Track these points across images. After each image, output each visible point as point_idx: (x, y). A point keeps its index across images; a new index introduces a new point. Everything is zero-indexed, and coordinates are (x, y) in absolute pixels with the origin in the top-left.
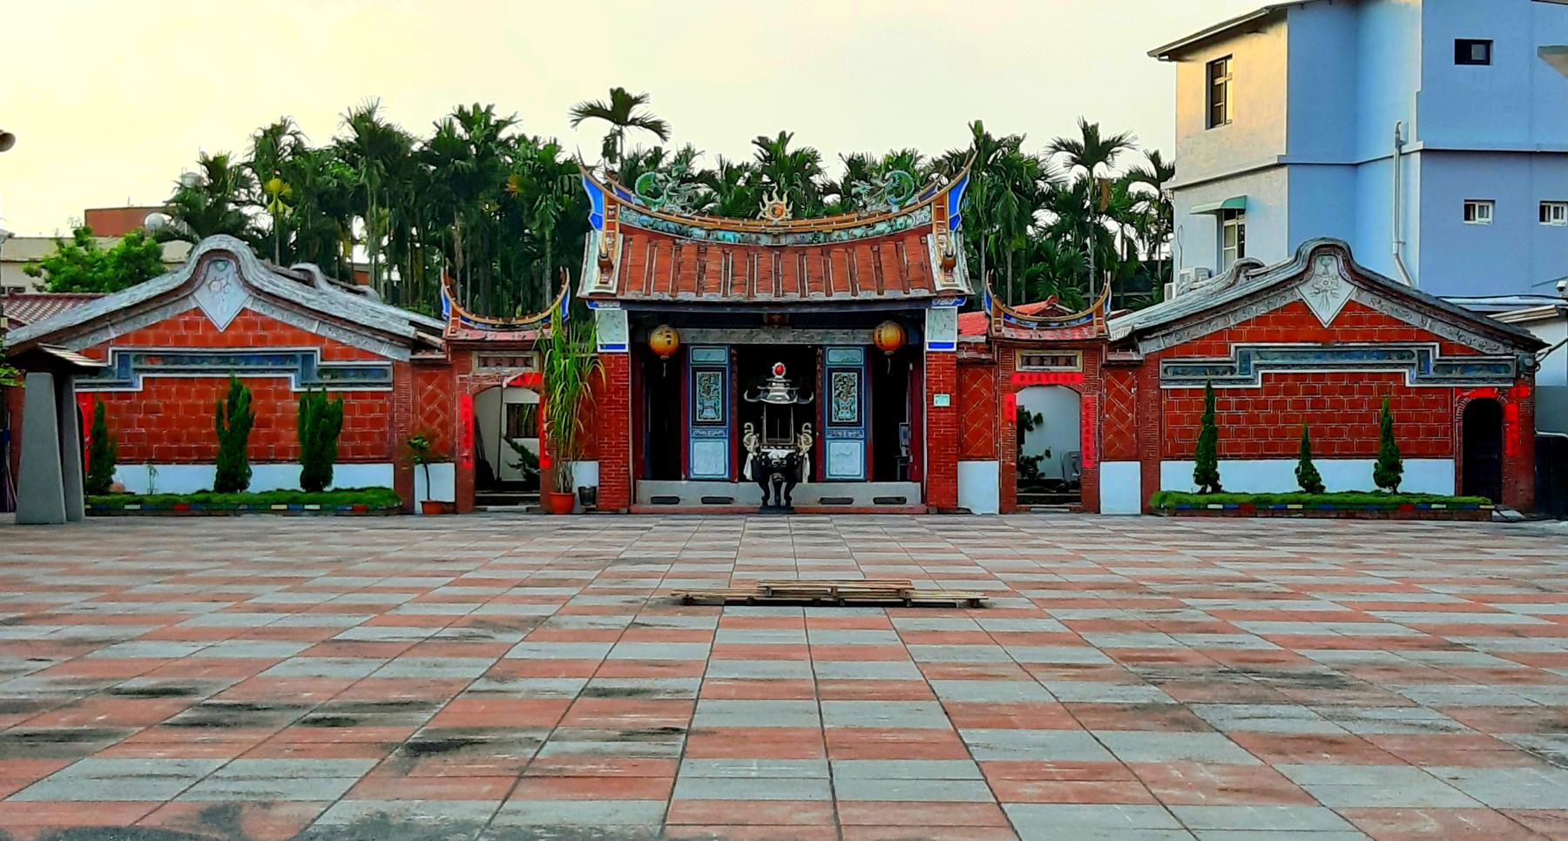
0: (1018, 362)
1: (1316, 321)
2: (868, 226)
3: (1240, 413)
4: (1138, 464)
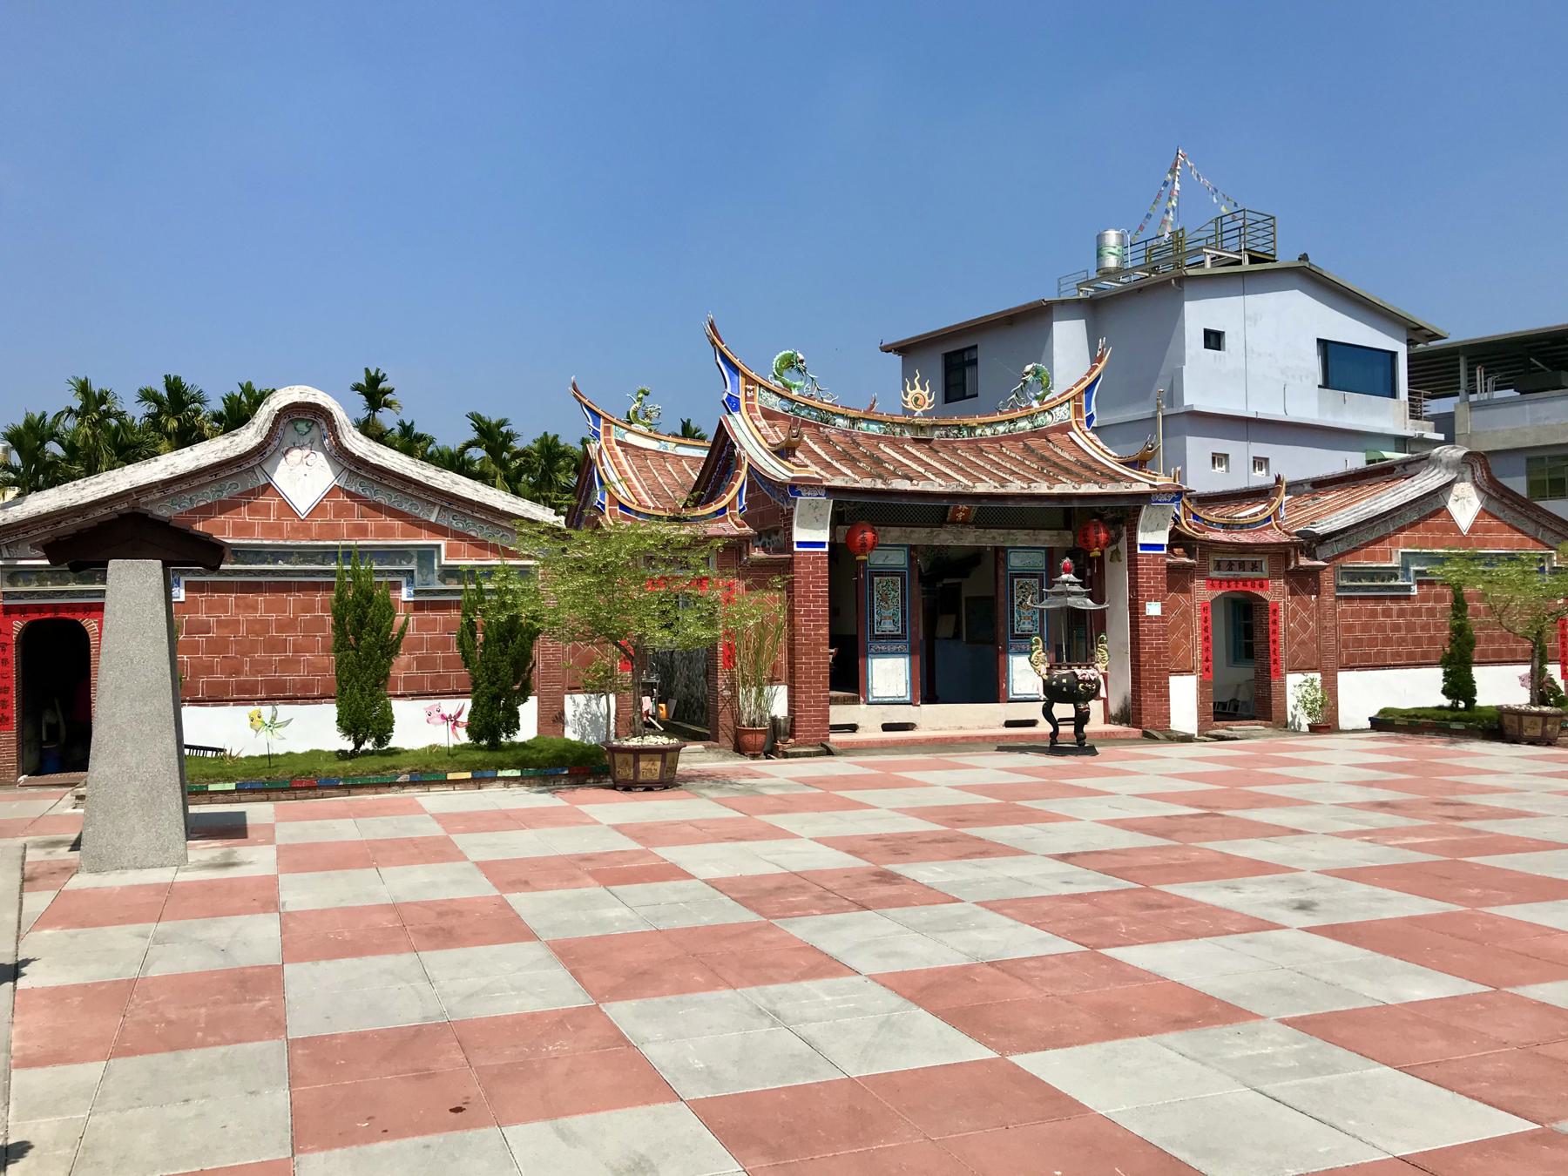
0: (1212, 566)
1: (1457, 529)
2: (1011, 421)
3: (1401, 621)
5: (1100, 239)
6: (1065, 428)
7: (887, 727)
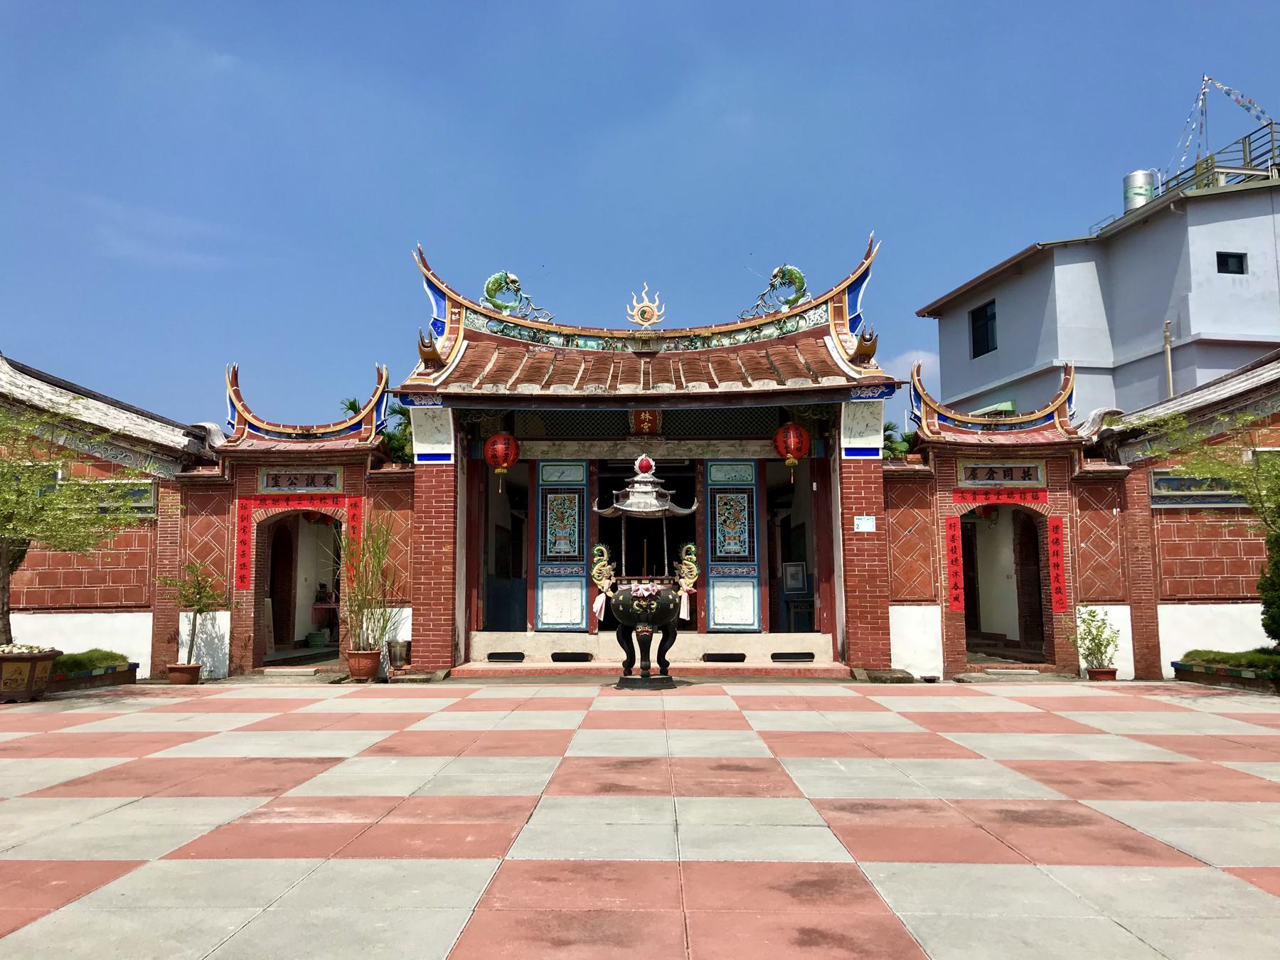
0: (961, 475)
2: (753, 329)
4: (1128, 608)
5: (1127, 182)
6: (820, 332)
7: (557, 657)
